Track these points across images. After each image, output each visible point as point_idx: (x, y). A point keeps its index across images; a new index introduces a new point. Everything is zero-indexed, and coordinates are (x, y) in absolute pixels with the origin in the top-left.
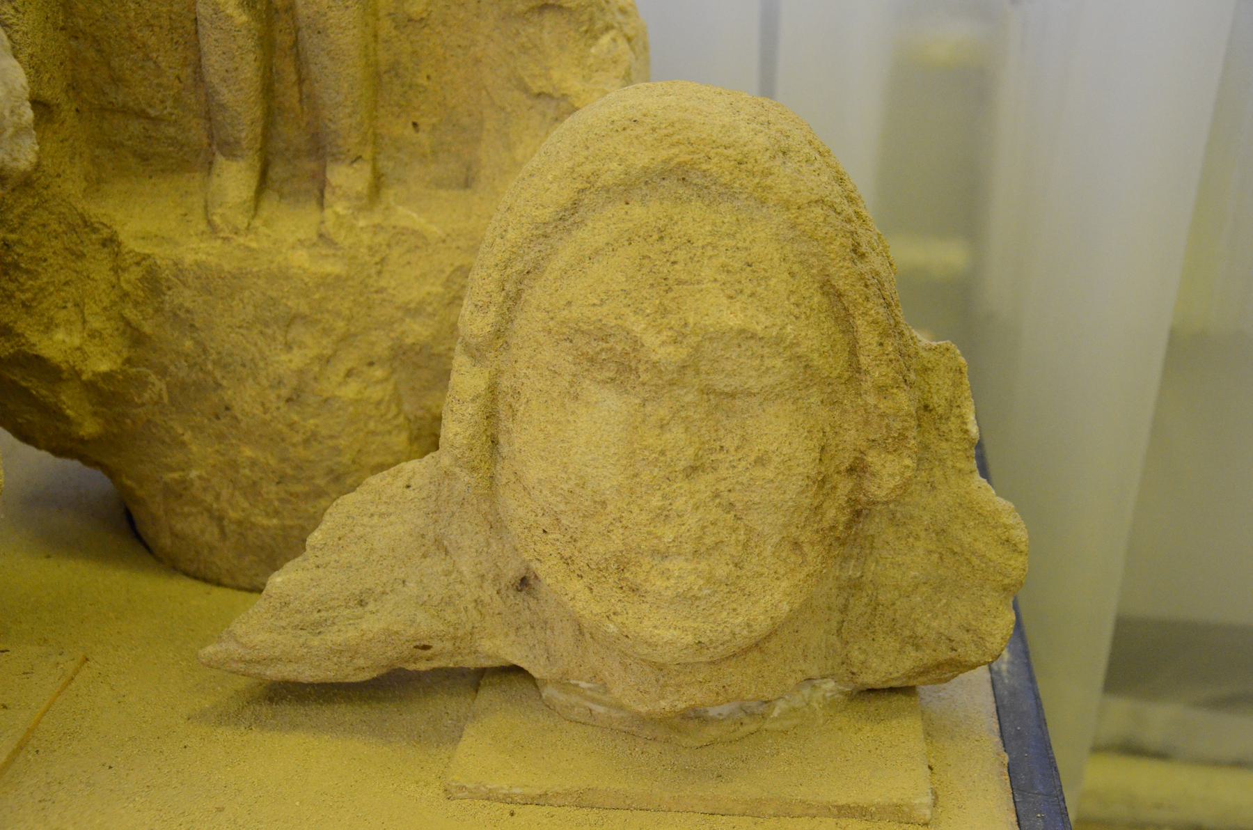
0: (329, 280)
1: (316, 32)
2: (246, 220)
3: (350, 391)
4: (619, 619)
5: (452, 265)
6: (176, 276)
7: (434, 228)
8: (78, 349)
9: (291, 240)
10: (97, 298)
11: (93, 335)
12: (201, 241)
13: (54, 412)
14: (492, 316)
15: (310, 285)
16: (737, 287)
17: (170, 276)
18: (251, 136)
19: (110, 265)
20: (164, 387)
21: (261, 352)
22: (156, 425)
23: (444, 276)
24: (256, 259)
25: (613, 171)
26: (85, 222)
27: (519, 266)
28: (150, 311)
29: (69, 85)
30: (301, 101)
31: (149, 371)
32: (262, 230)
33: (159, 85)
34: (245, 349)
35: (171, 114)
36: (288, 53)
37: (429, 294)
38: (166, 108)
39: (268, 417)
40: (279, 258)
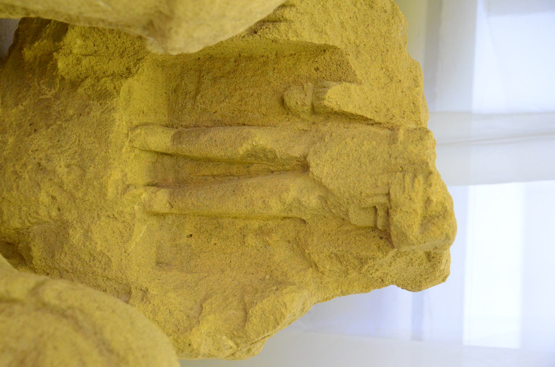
0: (104, 190)
1: (234, 190)
2: (138, 146)
3: (44, 198)
5: (112, 256)
6: (107, 108)
8: (71, 52)
10: (99, 63)
11: (79, 60)
12: (126, 122)
13: (37, 36)
15: (101, 180)
17: (107, 105)
18: (184, 150)
19: (116, 71)
20: (48, 97)
21: (66, 151)
22: (28, 91)
24: (116, 151)
26: (140, 60)
27: (80, 317)
28: (89, 93)
29: (212, 56)
30: (204, 175)
31: (57, 89)
32: (133, 155)
33: (212, 102)
34: (67, 143)
35: (198, 107)
36: (227, 171)
37: (96, 243)
38: (201, 104)
39: (30, 152)
40: (116, 164)
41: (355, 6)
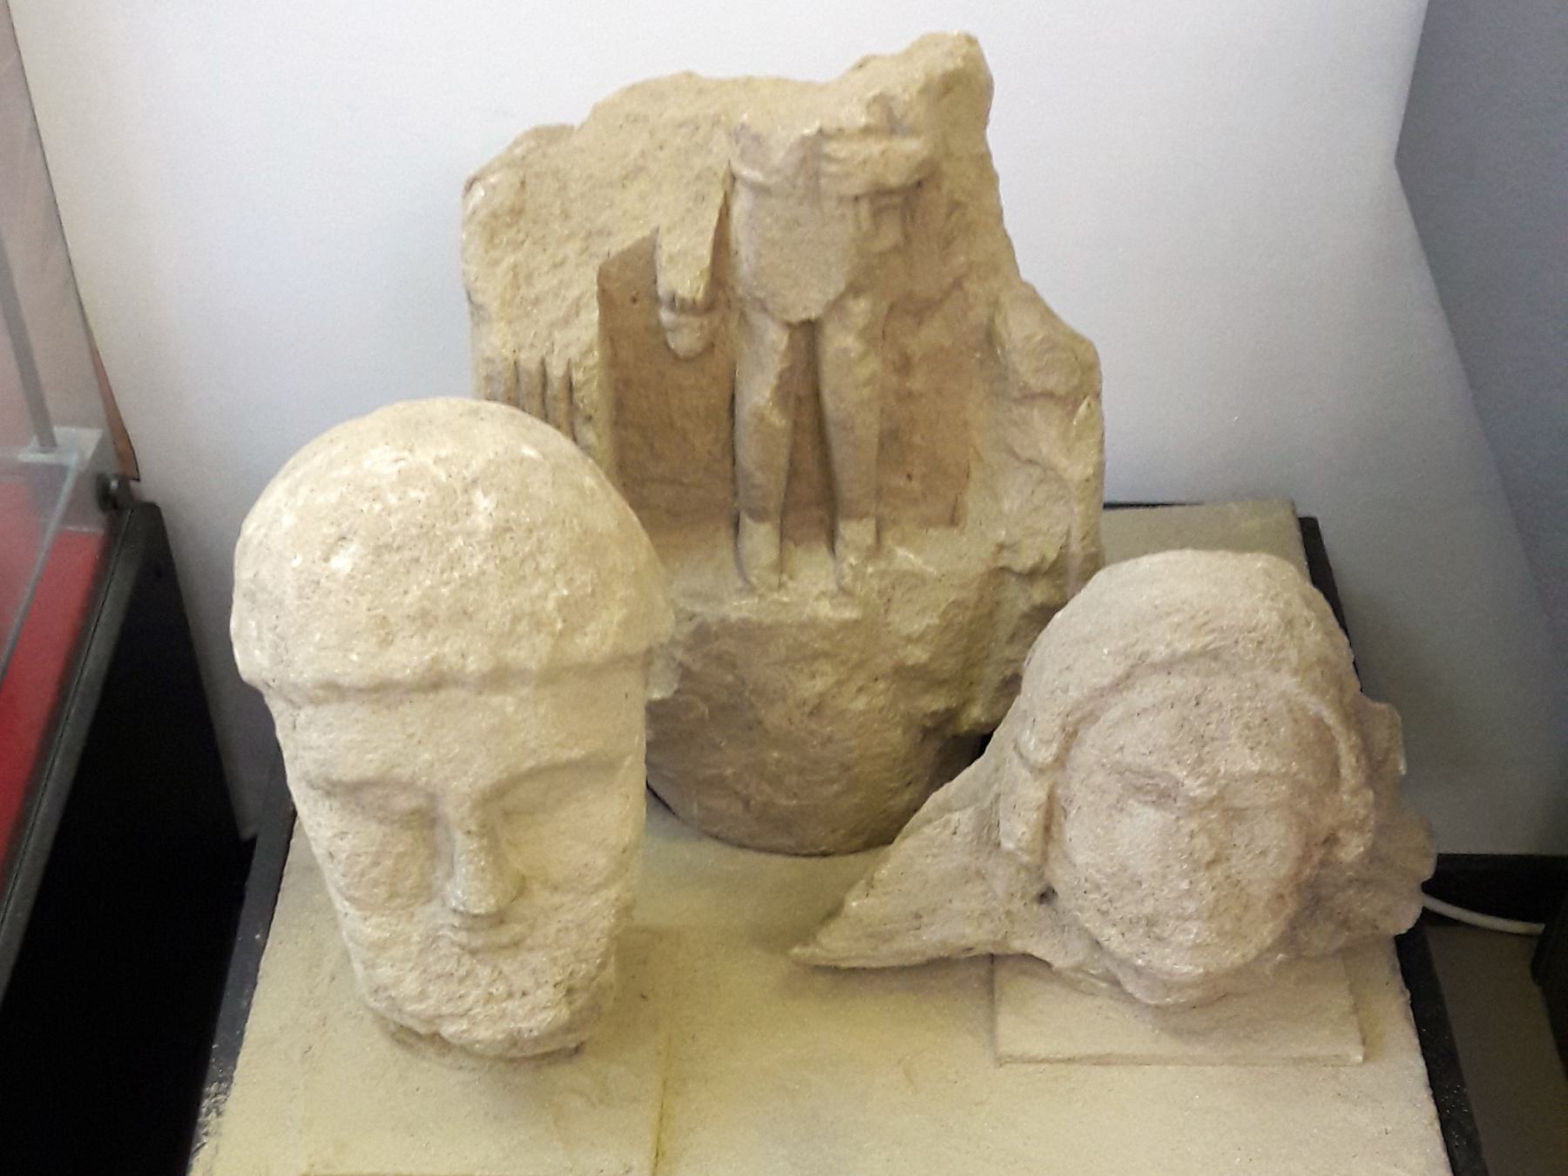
3: (860, 704)
4: (1147, 957)
7: (931, 569)
9: (815, 591)
14: (1054, 748)
16: (1257, 739)
23: (941, 610)
25: (1161, 652)
27: (1078, 715)
41: (523, 243)
